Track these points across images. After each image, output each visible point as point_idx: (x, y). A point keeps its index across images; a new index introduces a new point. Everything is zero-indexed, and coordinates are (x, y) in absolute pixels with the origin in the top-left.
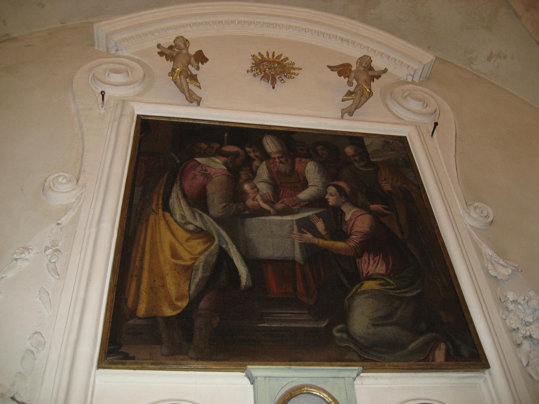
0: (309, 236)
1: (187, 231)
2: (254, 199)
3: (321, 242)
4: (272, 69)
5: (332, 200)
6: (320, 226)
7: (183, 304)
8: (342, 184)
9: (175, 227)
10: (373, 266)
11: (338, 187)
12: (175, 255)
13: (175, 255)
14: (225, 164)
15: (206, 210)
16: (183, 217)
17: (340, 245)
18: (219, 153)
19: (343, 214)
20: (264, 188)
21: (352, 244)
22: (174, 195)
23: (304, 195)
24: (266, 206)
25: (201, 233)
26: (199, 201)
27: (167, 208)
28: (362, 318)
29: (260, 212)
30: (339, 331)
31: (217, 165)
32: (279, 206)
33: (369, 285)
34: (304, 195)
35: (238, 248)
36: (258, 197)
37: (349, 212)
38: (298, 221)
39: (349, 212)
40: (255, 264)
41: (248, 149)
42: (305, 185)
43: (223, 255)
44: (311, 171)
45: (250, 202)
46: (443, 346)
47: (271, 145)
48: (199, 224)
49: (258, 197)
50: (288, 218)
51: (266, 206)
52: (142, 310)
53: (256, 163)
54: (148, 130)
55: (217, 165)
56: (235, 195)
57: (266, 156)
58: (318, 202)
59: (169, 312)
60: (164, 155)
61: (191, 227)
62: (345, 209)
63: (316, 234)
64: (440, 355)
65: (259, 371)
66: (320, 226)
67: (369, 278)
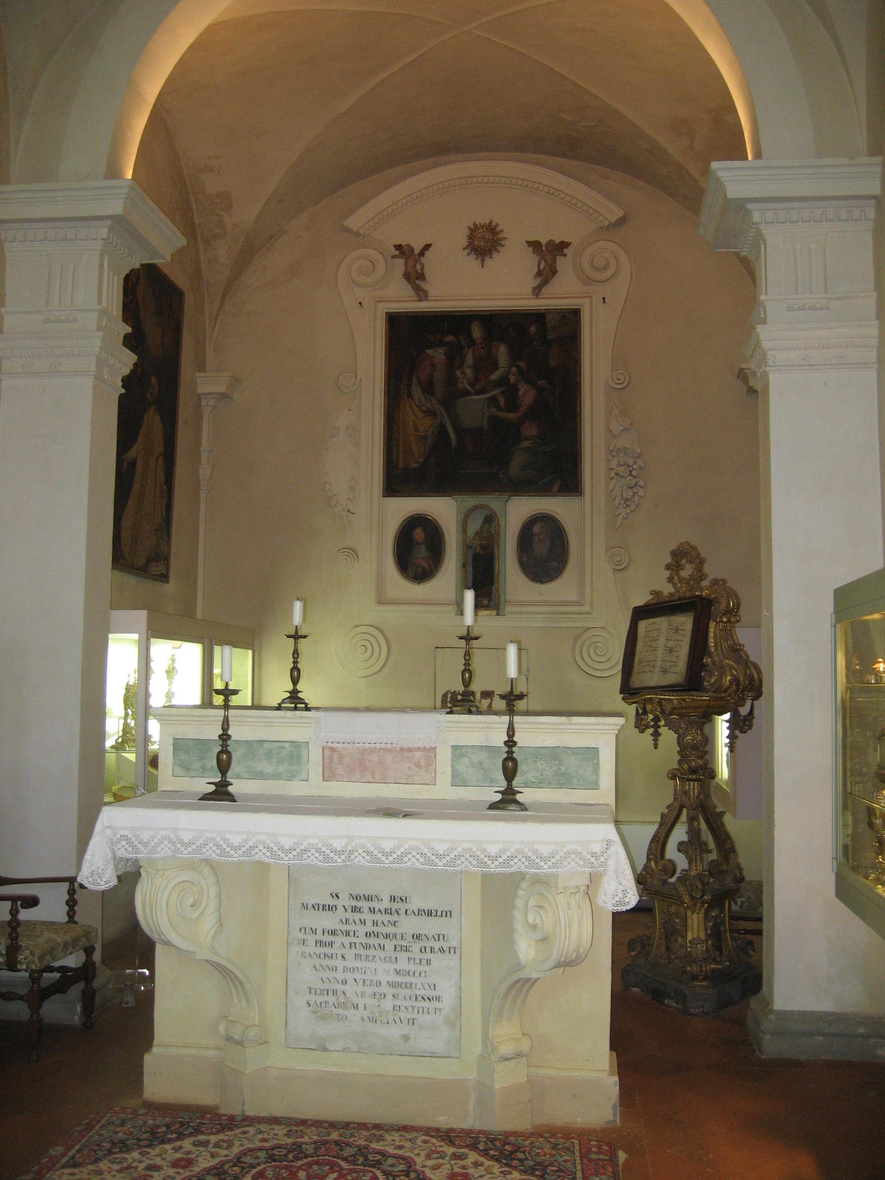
0: (494, 410)
1: (423, 411)
2: (462, 383)
3: (500, 414)
4: (171, 672)
5: (512, 379)
6: (502, 401)
7: (421, 460)
8: (522, 364)
9: (415, 409)
10: (530, 430)
11: (518, 367)
12: (416, 429)
13: (416, 429)
14: (445, 354)
15: (433, 395)
16: (419, 400)
17: (512, 415)
18: (442, 344)
19: (518, 390)
20: (469, 372)
21: (520, 415)
22: (413, 385)
23: (494, 377)
24: (469, 388)
25: (431, 413)
26: (428, 388)
27: (410, 395)
28: (517, 464)
29: (466, 393)
30: (503, 474)
31: (438, 354)
32: (477, 387)
33: (525, 444)
34: (494, 377)
35: (451, 422)
36: (465, 381)
37: (523, 388)
38: (489, 399)
39: (523, 388)
40: (459, 431)
41: (461, 337)
42: (496, 367)
43: (442, 427)
44: (502, 353)
45: (460, 386)
46: (559, 482)
47: (477, 332)
48: (429, 405)
49: (465, 381)
50: (482, 396)
51: (469, 388)
52: (401, 466)
53: (466, 350)
54: (394, 321)
55: (438, 354)
56: (451, 381)
57: (472, 343)
58: (503, 381)
59: (415, 466)
60: (412, 339)
61: (424, 408)
62: (520, 386)
63: (499, 409)
64: (556, 488)
65: (460, 498)
66: (502, 401)
67: (526, 439)
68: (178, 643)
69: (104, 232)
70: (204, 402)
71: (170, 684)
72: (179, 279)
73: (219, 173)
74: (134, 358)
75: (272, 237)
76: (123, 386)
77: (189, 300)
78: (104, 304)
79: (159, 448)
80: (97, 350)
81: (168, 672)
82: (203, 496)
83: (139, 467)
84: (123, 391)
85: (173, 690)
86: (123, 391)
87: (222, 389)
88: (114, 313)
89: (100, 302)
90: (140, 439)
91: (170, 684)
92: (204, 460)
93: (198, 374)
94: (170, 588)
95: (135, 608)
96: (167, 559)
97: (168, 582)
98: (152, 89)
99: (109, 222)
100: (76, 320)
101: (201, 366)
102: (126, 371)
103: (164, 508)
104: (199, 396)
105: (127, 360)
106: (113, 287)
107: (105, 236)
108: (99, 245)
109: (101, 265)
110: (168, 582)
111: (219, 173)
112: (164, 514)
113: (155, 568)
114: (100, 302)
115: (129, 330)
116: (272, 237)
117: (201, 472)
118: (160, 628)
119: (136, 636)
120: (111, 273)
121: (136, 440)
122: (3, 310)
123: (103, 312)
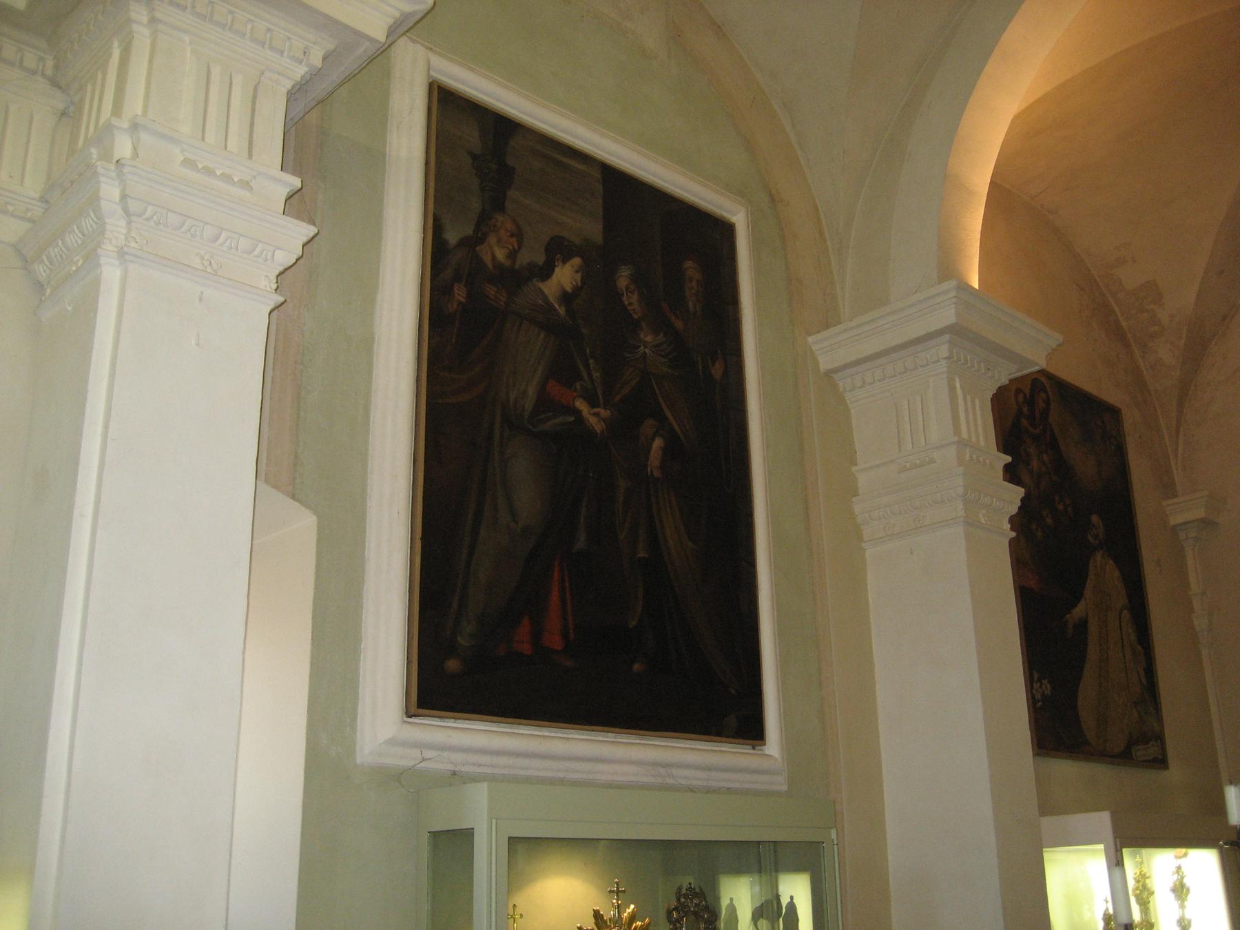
68: (1183, 850)
69: (944, 351)
70: (1182, 536)
71: (1182, 906)
72: (1110, 394)
73: (1134, 261)
74: (1021, 491)
75: (1224, 318)
76: (1012, 529)
77: (1131, 419)
78: (965, 435)
79: (1120, 598)
80: (960, 491)
81: (1174, 890)
82: (1204, 652)
83: (1093, 628)
84: (1013, 534)
85: (1187, 916)
86: (1013, 534)
87: (1200, 513)
88: (982, 443)
89: (957, 431)
90: (1088, 592)
91: (1182, 906)
92: (1196, 605)
93: (1164, 503)
94: (1175, 774)
95: (1096, 809)
96: (1160, 738)
97: (1166, 768)
98: (980, 179)
99: (947, 337)
100: (932, 461)
101: (1168, 489)
102: (1014, 509)
103: (1142, 673)
104: (1174, 530)
105: (1013, 496)
106: (974, 414)
107: (946, 354)
108: (943, 366)
109: (952, 389)
110: (1166, 768)
111: (1134, 261)
112: (1144, 681)
113: (1140, 752)
114: (957, 431)
115: (1009, 459)
116: (1224, 318)
117: (1196, 623)
118: (1137, 830)
119: (1101, 847)
120: (969, 397)
121: (1082, 595)
122: (854, 469)
123: (962, 444)
